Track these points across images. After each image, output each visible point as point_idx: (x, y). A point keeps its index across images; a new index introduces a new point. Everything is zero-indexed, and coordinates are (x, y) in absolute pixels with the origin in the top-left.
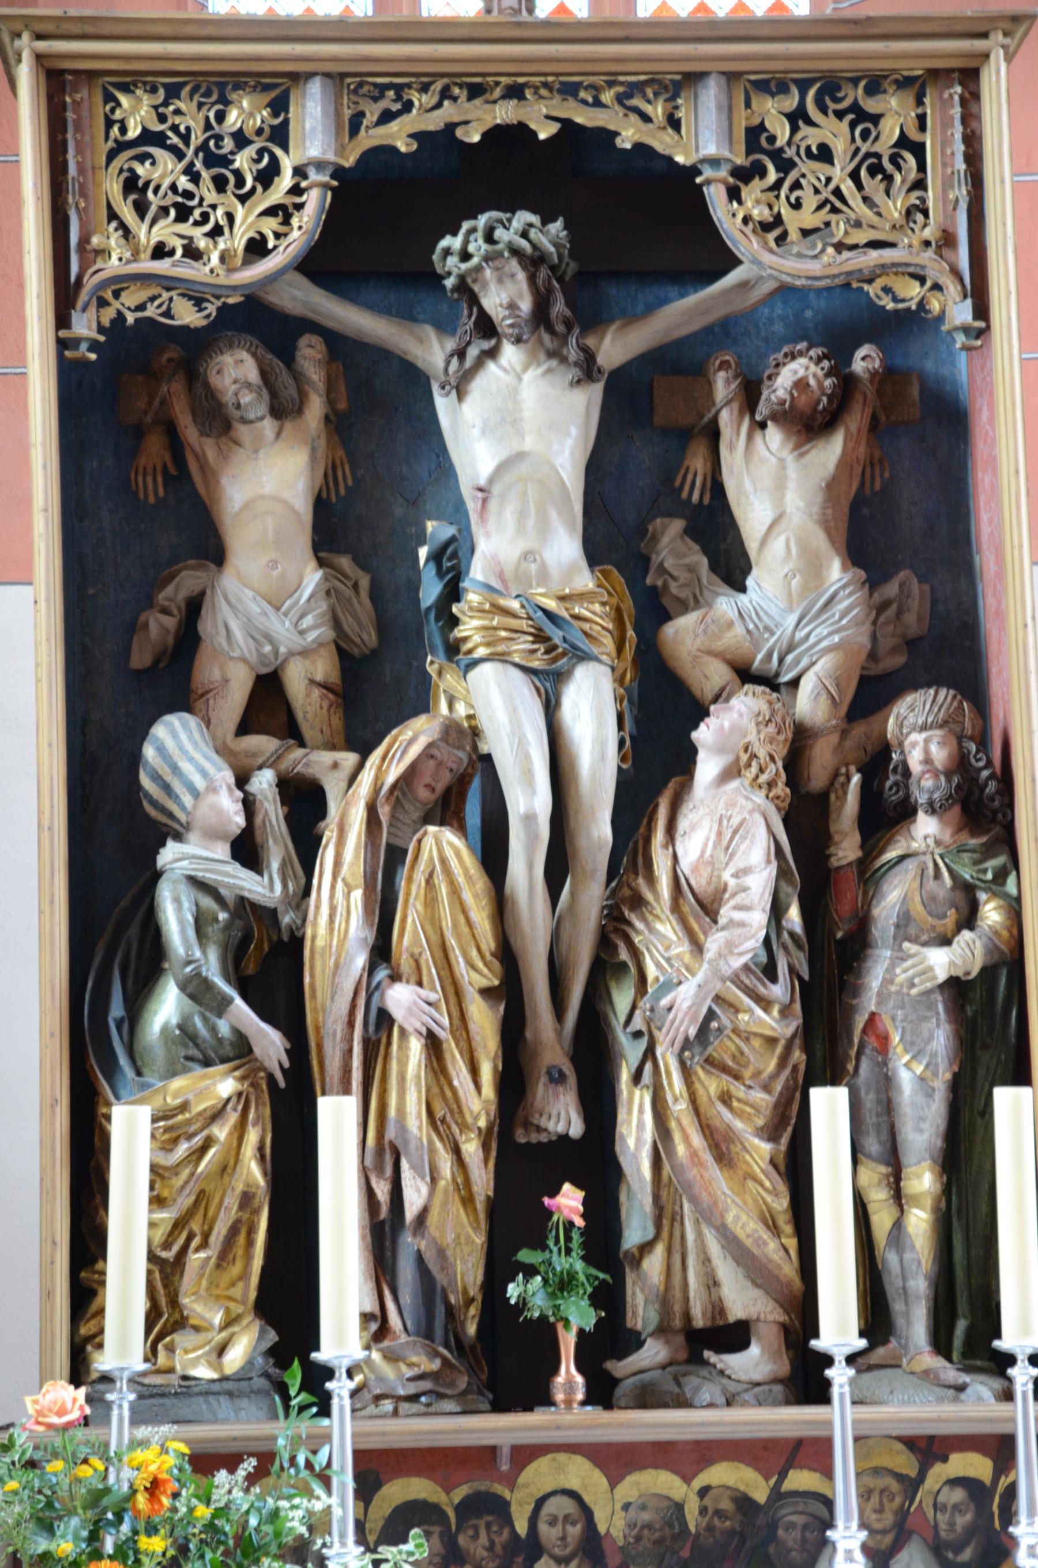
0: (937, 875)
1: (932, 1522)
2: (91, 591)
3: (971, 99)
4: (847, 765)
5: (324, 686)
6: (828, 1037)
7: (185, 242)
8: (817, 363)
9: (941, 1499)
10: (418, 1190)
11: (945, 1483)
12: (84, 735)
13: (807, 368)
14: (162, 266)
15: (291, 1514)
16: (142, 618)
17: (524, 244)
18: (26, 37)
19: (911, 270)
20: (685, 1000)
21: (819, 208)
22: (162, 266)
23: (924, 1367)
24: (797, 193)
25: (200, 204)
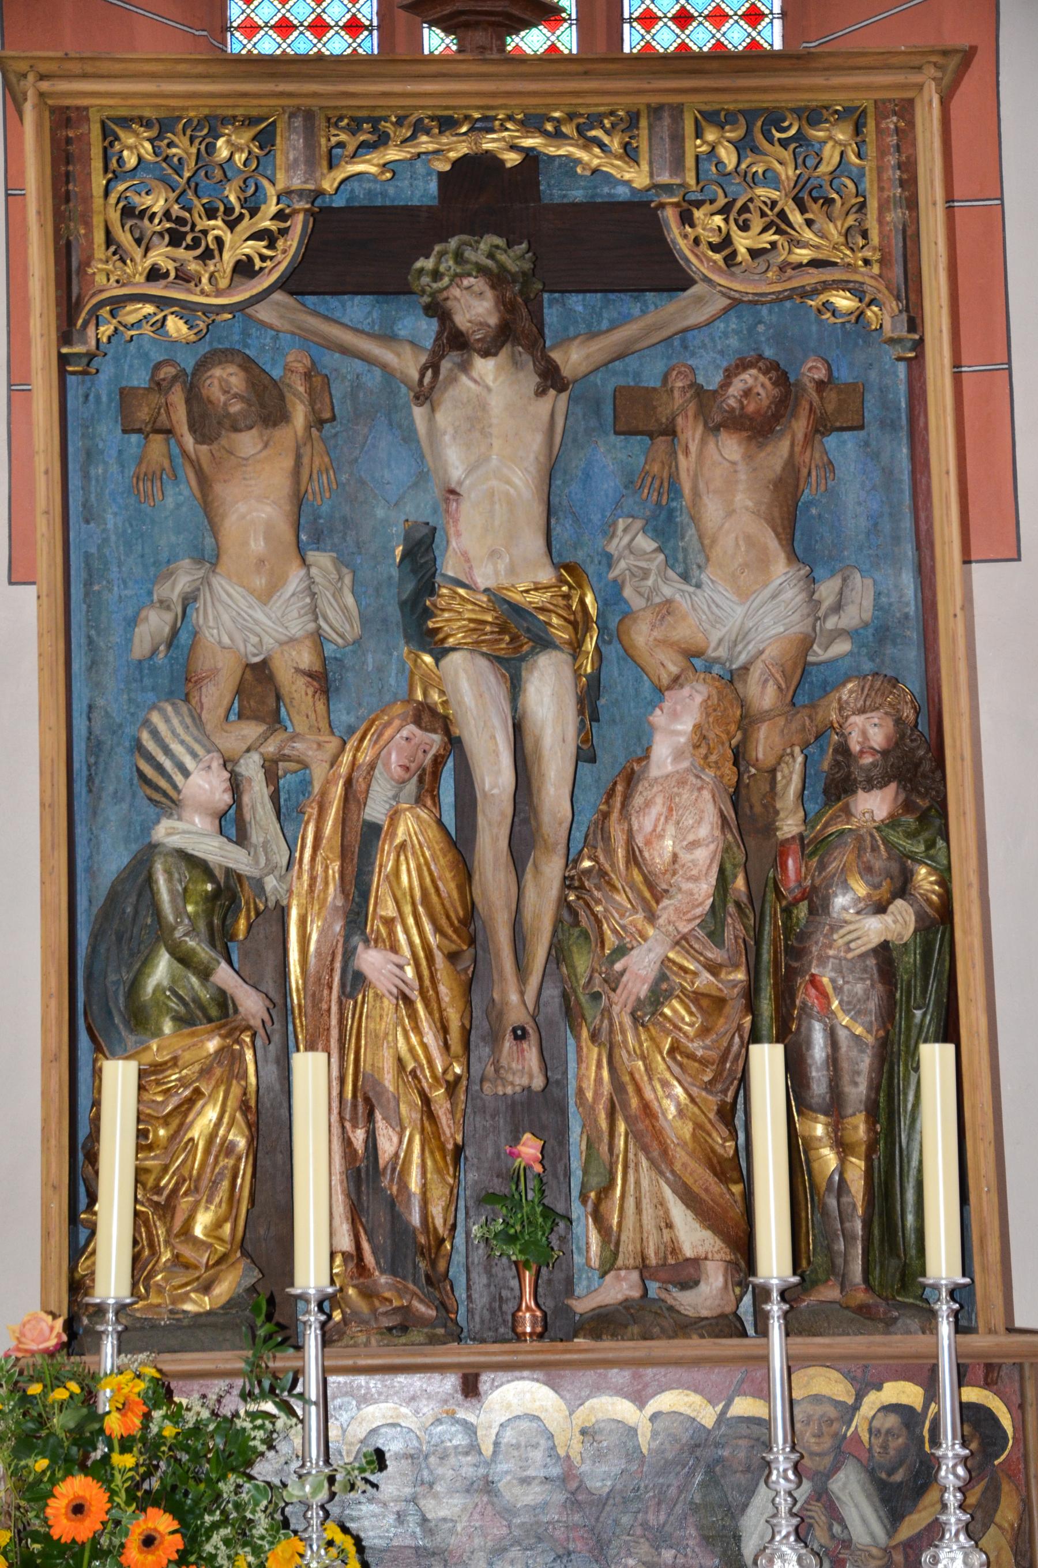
0: (875, 849)
1: (867, 1446)
2: (96, 588)
3: (906, 135)
4: (792, 746)
5: (310, 675)
6: (775, 996)
7: (177, 265)
8: (764, 374)
9: (876, 1424)
10: (390, 1139)
11: (879, 1410)
12: (89, 719)
13: (756, 379)
14: (156, 290)
15: (253, 1434)
16: (143, 614)
17: (489, 263)
18: (31, 78)
19: (851, 285)
20: (641, 967)
21: (764, 230)
22: (156, 290)
23: (858, 1302)
24: (747, 216)
25: (192, 229)
